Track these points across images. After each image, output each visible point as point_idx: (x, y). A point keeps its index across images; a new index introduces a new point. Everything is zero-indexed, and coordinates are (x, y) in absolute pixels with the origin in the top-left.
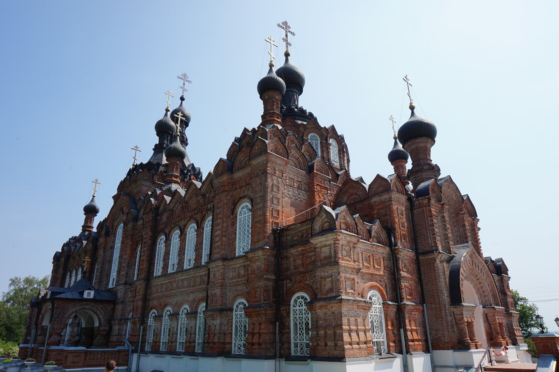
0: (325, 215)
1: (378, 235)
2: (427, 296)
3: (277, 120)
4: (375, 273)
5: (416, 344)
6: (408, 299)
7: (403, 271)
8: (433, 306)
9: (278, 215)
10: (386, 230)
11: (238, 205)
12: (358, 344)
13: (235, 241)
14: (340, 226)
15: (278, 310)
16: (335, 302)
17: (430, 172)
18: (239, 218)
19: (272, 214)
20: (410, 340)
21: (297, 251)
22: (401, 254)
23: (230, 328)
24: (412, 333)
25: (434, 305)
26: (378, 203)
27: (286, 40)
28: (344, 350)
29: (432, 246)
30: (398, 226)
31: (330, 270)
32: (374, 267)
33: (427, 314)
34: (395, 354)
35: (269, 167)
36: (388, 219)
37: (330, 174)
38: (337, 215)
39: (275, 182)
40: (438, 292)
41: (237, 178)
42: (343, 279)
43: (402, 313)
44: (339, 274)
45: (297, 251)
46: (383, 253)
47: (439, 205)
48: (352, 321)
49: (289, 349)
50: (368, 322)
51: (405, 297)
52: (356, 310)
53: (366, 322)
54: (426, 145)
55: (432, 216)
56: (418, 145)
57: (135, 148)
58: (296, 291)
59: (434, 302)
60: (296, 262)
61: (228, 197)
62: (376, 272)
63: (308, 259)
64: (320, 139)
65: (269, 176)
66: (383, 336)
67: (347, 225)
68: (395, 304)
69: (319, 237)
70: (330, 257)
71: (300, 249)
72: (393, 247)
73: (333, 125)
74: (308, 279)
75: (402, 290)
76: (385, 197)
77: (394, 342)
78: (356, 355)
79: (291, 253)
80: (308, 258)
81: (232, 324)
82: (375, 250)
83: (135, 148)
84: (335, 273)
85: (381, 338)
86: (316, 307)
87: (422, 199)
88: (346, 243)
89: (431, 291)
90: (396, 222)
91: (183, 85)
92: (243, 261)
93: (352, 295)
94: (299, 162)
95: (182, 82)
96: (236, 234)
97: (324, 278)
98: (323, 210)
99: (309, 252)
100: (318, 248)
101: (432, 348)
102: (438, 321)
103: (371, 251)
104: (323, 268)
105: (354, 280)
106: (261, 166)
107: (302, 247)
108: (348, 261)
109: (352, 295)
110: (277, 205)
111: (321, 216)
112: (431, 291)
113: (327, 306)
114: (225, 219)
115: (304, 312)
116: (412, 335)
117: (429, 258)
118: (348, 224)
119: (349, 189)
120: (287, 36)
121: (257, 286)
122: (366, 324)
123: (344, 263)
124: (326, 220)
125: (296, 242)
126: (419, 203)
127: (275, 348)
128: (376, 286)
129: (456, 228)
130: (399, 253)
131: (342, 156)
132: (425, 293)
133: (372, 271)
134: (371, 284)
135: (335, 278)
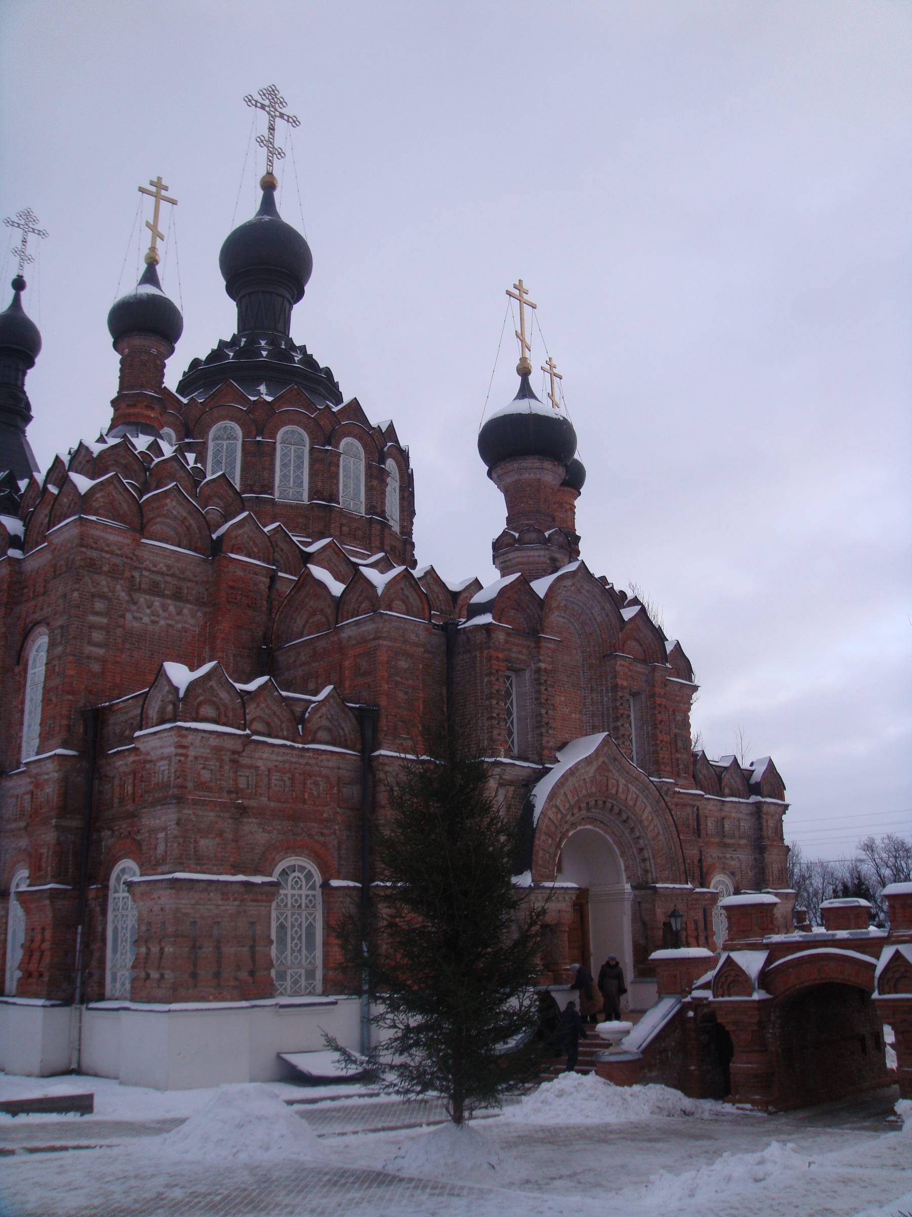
11: (30, 642)
21: (126, 765)
22: (387, 768)
27: (268, 143)
45: (126, 765)
46: (339, 768)
52: (220, 902)
54: (538, 476)
57: (153, 189)
58: (119, 857)
73: (355, 399)
82: (312, 761)
83: (153, 189)
88: (208, 751)
91: (28, 240)
95: (18, 234)
103: (300, 764)
115: (304, 902)
120: (272, 129)
121: (42, 843)
129: (594, 695)
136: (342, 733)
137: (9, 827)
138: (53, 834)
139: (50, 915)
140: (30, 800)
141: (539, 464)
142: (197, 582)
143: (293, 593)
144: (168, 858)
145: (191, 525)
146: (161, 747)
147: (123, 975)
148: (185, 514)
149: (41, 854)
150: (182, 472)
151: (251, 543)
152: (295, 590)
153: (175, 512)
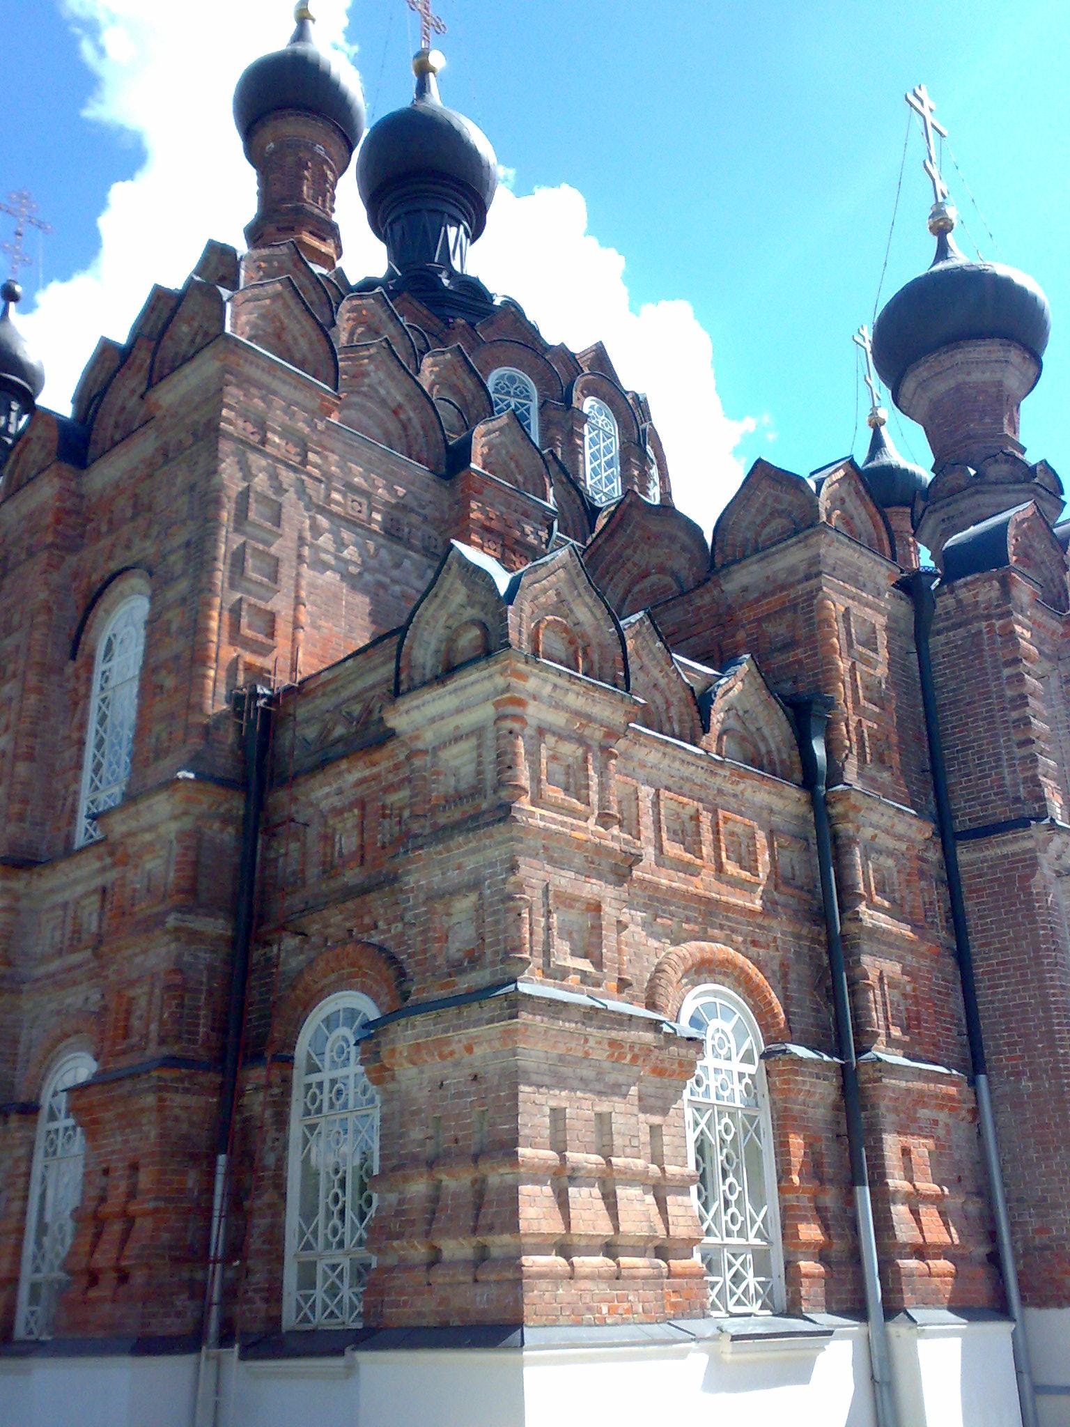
0: (463, 591)
1: (746, 729)
2: (995, 1039)
3: (315, 243)
4: (724, 898)
5: (934, 1270)
6: (891, 1042)
7: (872, 906)
8: (1026, 1084)
9: (271, 635)
10: (788, 709)
12: (610, 1249)
13: (77, 779)
14: (534, 640)
15: (230, 1094)
16: (486, 1016)
17: (1014, 491)
18: (104, 673)
19: (235, 626)
20: (905, 1245)
21: (340, 792)
23: (16, 1206)
24: (915, 1213)
25: (1031, 1079)
26: (756, 595)
28: (516, 1281)
29: (1017, 800)
30: (849, 693)
31: (473, 852)
32: (720, 868)
33: (995, 1124)
34: (825, 1320)
35: (231, 408)
36: (799, 662)
37: (551, 491)
38: (514, 586)
39: (261, 481)
40: (1053, 1032)
41: (104, 489)
42: (533, 895)
43: (865, 1109)
44: (514, 868)
47: (1055, 624)
48: (578, 1124)
49: (274, 1293)
50: (677, 1141)
51: (882, 1031)
53: (666, 1139)
54: (998, 376)
55: (1017, 661)
56: (961, 378)
59: (1030, 1063)
60: (333, 847)
61: (55, 578)
62: (733, 895)
63: (386, 822)
64: (541, 395)
65: (225, 446)
66: (764, 1222)
67: (571, 642)
68: (826, 1058)
69: (427, 697)
70: (476, 791)
71: (352, 777)
72: (822, 788)
74: (381, 924)
75: (866, 992)
76: (792, 557)
77: (823, 1258)
78: (589, 1309)
79: (311, 805)
80: (384, 816)
81: (28, 1183)
84: (492, 865)
85: (751, 1234)
86: (393, 1051)
87: (972, 583)
89: (1013, 1014)
90: (837, 670)
92: (97, 865)
93: (582, 982)
94: (405, 428)
96: (81, 743)
97: (447, 895)
98: (455, 566)
99: (391, 788)
100: (425, 752)
101: (1023, 1298)
102: (1048, 1158)
104: (440, 847)
105: (596, 908)
106: (196, 409)
107: (360, 764)
108: (572, 812)
109: (582, 982)
110: (268, 588)
111: (445, 597)
112: (1013, 1014)
113: (448, 1042)
114: (32, 679)
116: (918, 1221)
117: (1005, 856)
118: (583, 636)
119: (629, 552)
121: (135, 975)
122: (666, 1150)
123: (542, 818)
124: (470, 613)
125: (340, 748)
126: (959, 601)
127: (199, 1291)
128: (728, 962)
130: (851, 814)
131: (636, 473)
132: (983, 1024)
133: (704, 884)
134: (702, 950)
135: (493, 895)
136: (763, 750)
137: (41, 971)
138: (164, 950)
139: (153, 1134)
140: (97, 906)
141: (1002, 354)
142: (425, 518)
143: (600, 541)
144: (488, 952)
145: (410, 419)
146: (459, 711)
147: (334, 1267)
148: (399, 398)
149: (132, 1000)
150: (390, 326)
151: (513, 465)
152: (604, 536)
153: (382, 392)
